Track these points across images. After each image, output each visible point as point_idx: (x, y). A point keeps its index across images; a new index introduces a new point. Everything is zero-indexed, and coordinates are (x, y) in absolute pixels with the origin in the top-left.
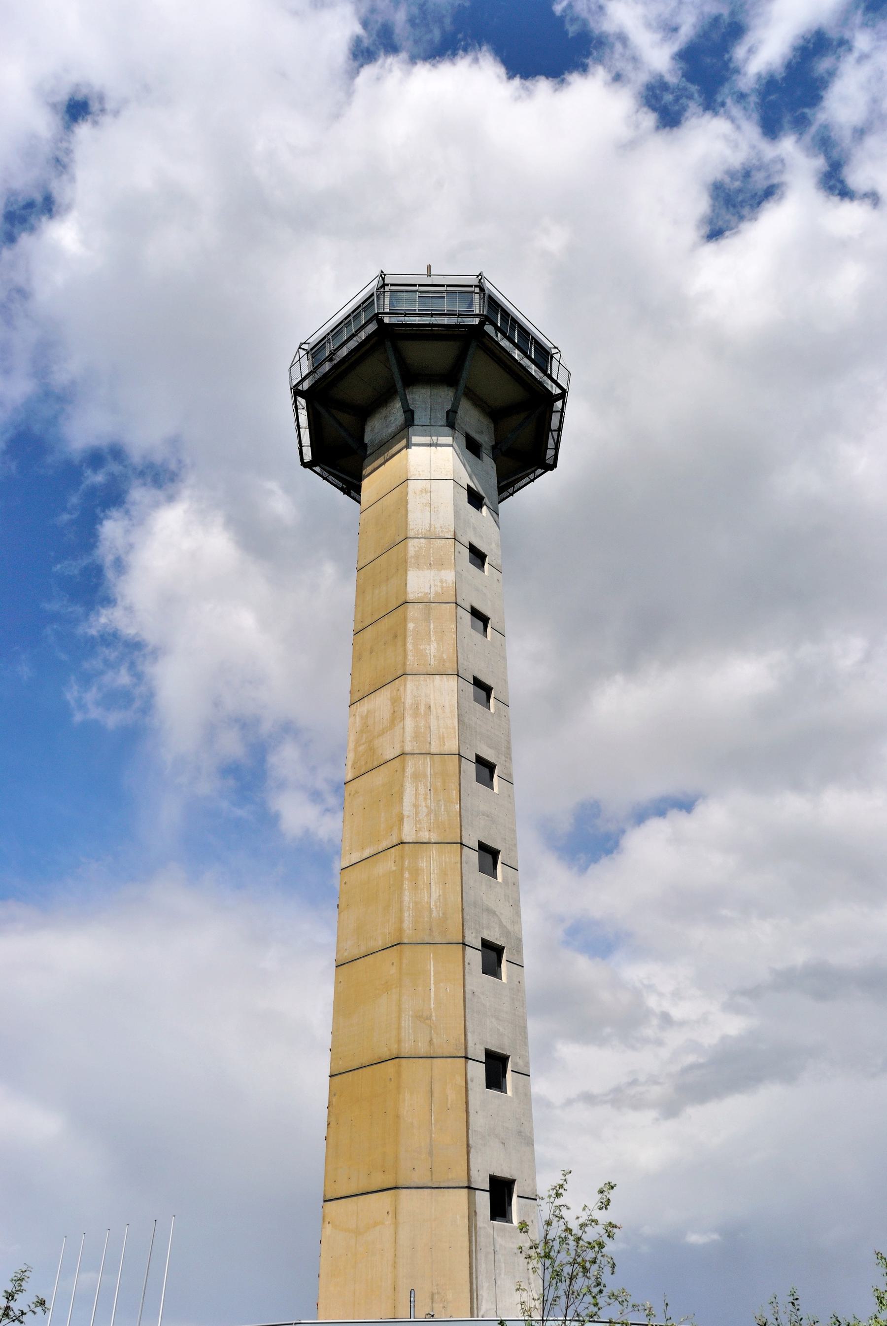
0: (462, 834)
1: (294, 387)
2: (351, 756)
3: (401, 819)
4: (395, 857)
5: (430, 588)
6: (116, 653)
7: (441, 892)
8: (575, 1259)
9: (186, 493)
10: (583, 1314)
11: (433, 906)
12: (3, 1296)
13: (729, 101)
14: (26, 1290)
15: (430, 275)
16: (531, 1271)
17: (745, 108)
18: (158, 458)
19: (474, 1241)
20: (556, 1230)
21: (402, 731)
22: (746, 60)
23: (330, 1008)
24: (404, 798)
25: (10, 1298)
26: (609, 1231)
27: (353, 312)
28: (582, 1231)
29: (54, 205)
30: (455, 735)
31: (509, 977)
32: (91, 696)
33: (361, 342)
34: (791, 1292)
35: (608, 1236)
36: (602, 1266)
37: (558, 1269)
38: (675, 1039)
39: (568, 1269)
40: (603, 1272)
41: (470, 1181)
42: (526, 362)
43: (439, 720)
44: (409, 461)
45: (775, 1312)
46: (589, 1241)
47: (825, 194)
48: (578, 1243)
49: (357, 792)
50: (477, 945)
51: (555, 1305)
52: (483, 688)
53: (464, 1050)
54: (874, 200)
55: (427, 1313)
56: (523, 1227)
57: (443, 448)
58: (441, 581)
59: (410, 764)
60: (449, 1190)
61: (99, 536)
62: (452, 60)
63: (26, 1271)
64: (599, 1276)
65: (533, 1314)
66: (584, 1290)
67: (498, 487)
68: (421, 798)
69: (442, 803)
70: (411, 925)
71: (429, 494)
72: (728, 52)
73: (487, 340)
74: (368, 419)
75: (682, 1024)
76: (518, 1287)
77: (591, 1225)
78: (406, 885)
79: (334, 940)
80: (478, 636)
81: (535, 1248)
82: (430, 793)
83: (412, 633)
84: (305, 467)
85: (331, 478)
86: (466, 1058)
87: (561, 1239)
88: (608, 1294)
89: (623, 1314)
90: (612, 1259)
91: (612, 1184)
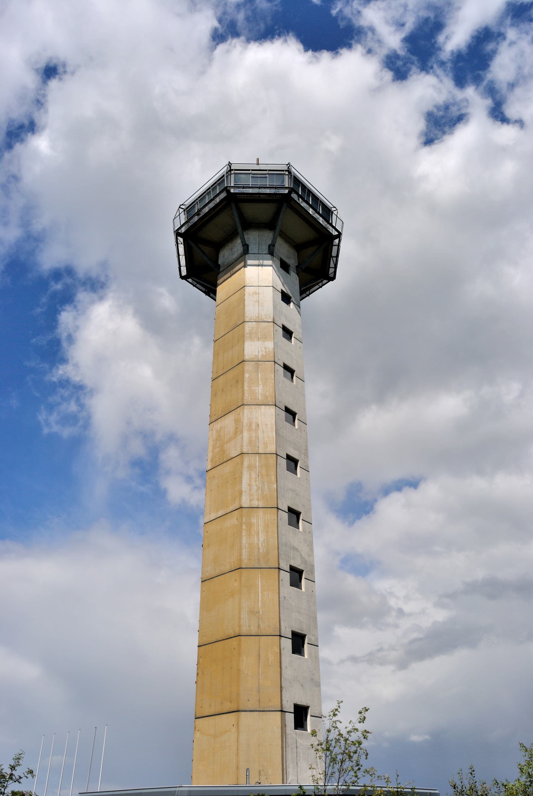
0: (278, 502)
1: (176, 231)
2: (210, 455)
3: (241, 493)
4: (237, 516)
5: (259, 352)
6: (68, 392)
7: (265, 537)
8: (344, 751)
9: (111, 295)
10: (349, 781)
11: (260, 545)
12: (9, 768)
13: (435, 66)
14: (22, 764)
15: (258, 164)
16: (318, 758)
17: (445, 70)
18: (94, 274)
19: (284, 741)
20: (333, 735)
21: (241, 439)
22: (445, 43)
23: (198, 607)
24: (243, 480)
25: (13, 769)
26: (364, 735)
27: (212, 186)
28: (348, 735)
29: (35, 126)
30: (274, 442)
31: (306, 588)
32: (53, 418)
33: (217, 204)
34: (470, 767)
35: (364, 738)
36: (360, 755)
37: (334, 757)
38: (405, 623)
39: (340, 757)
40: (360, 758)
41: (282, 707)
42: (316, 216)
43: (264, 433)
44: (246, 275)
45: (461, 778)
46: (352, 740)
47: (493, 120)
48: (346, 742)
49: (214, 477)
50: (287, 569)
51: (332, 777)
52: (291, 413)
53: (279, 632)
54: (521, 124)
55: (257, 781)
56: (314, 733)
57: (266, 267)
58: (265, 348)
59: (246, 460)
60: (269, 712)
61: (58, 321)
62: (271, 40)
63: (21, 754)
64: (358, 760)
65: (319, 782)
66: (350, 769)
67: (300, 291)
68: (253, 480)
69: (266, 483)
70: (247, 557)
71: (258, 295)
72: (434, 38)
73: (293, 202)
74: (221, 250)
75: (410, 615)
76: (310, 767)
77: (354, 731)
78: (244, 533)
79: (199, 566)
80: (287, 382)
81: (321, 745)
82: (259, 477)
83: (247, 380)
84: (182, 279)
85: (198, 285)
86: (280, 636)
87: (336, 740)
88: (363, 771)
89: (372, 781)
90: (366, 751)
91: (367, 708)
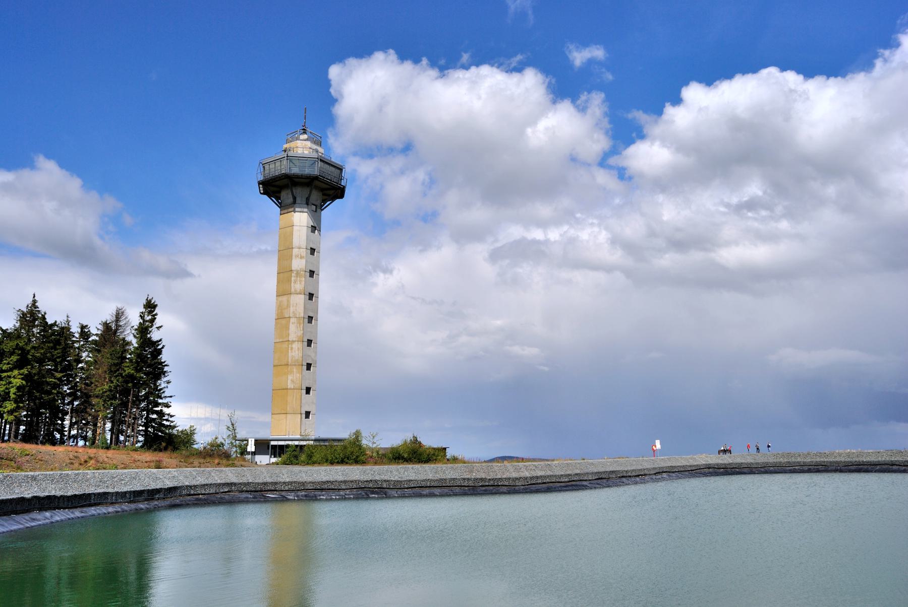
31: (313, 370)
78: (290, 351)
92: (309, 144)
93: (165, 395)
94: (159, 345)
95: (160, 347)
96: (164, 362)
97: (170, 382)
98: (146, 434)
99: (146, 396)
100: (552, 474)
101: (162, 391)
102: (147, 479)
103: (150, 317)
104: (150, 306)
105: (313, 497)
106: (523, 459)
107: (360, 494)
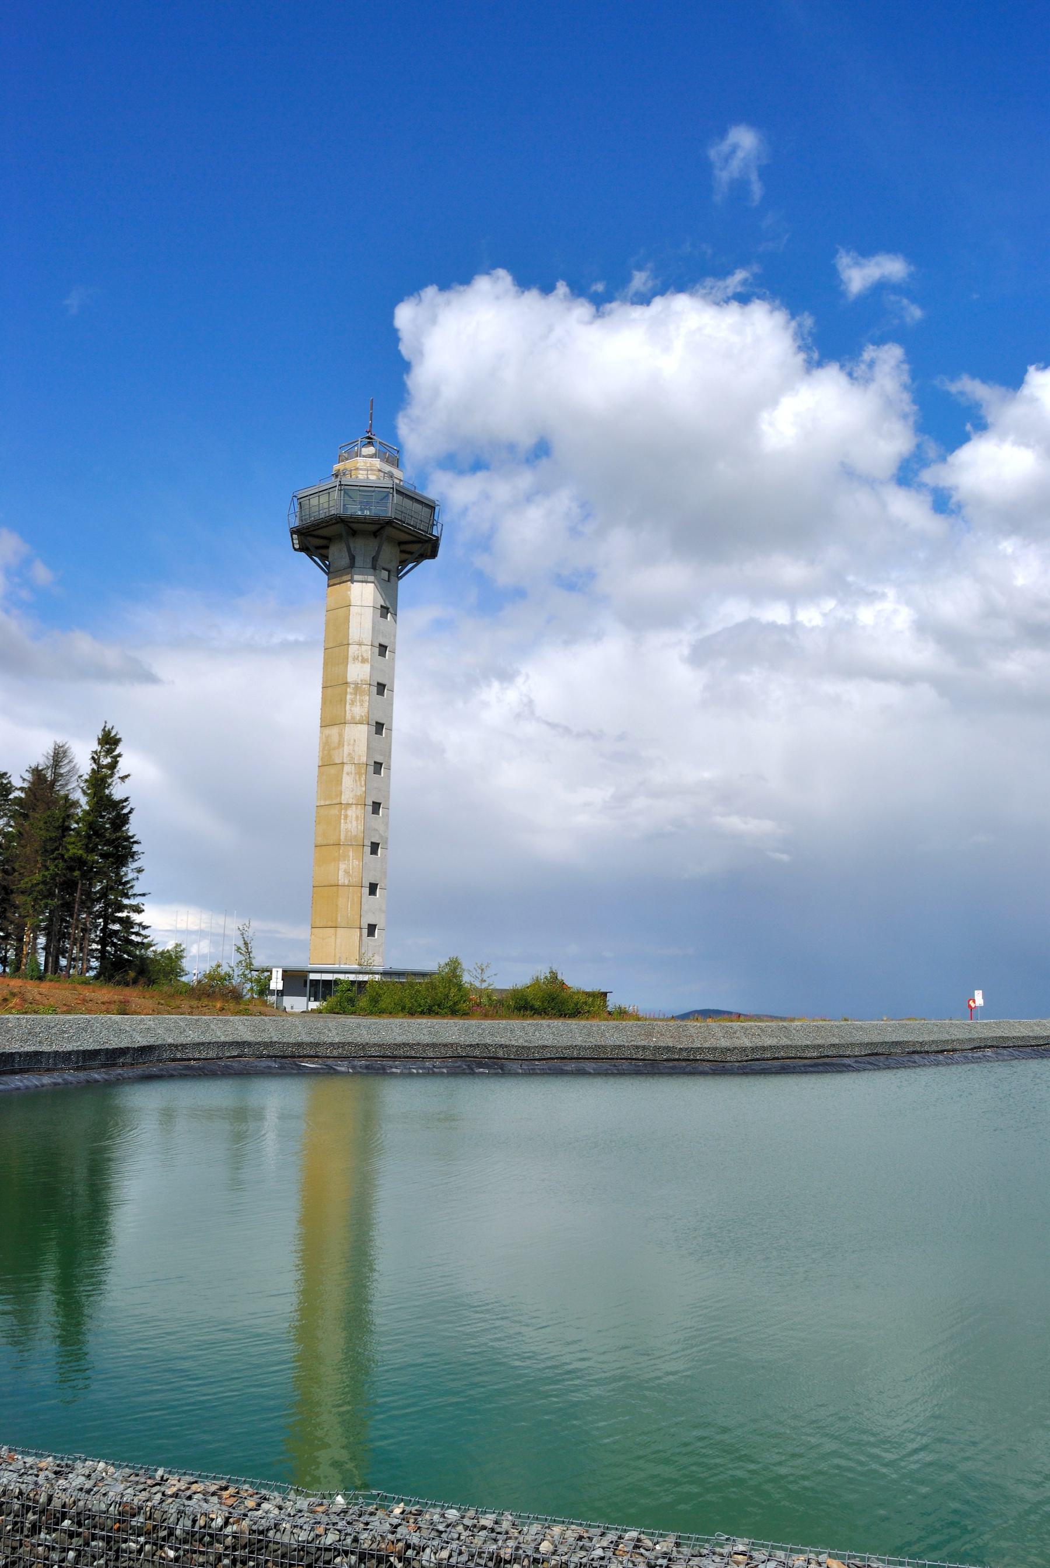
78: (342, 821)
92: (377, 462)
93: (134, 892)
94: (123, 807)
95: (125, 811)
96: (132, 837)
97: (143, 870)
98: (103, 956)
99: (104, 894)
100: (789, 1043)
101: (129, 886)
102: (105, 1032)
103: (109, 760)
104: (109, 741)
105: (379, 1069)
106: (739, 1015)
107: (459, 1067)
